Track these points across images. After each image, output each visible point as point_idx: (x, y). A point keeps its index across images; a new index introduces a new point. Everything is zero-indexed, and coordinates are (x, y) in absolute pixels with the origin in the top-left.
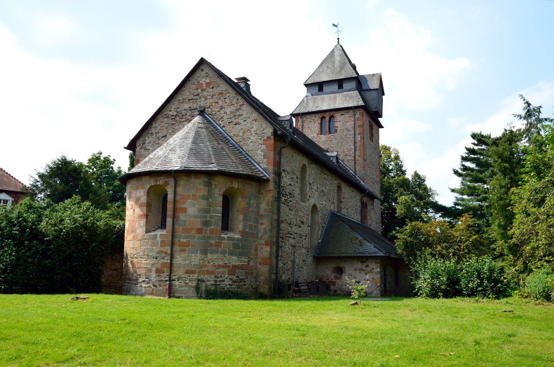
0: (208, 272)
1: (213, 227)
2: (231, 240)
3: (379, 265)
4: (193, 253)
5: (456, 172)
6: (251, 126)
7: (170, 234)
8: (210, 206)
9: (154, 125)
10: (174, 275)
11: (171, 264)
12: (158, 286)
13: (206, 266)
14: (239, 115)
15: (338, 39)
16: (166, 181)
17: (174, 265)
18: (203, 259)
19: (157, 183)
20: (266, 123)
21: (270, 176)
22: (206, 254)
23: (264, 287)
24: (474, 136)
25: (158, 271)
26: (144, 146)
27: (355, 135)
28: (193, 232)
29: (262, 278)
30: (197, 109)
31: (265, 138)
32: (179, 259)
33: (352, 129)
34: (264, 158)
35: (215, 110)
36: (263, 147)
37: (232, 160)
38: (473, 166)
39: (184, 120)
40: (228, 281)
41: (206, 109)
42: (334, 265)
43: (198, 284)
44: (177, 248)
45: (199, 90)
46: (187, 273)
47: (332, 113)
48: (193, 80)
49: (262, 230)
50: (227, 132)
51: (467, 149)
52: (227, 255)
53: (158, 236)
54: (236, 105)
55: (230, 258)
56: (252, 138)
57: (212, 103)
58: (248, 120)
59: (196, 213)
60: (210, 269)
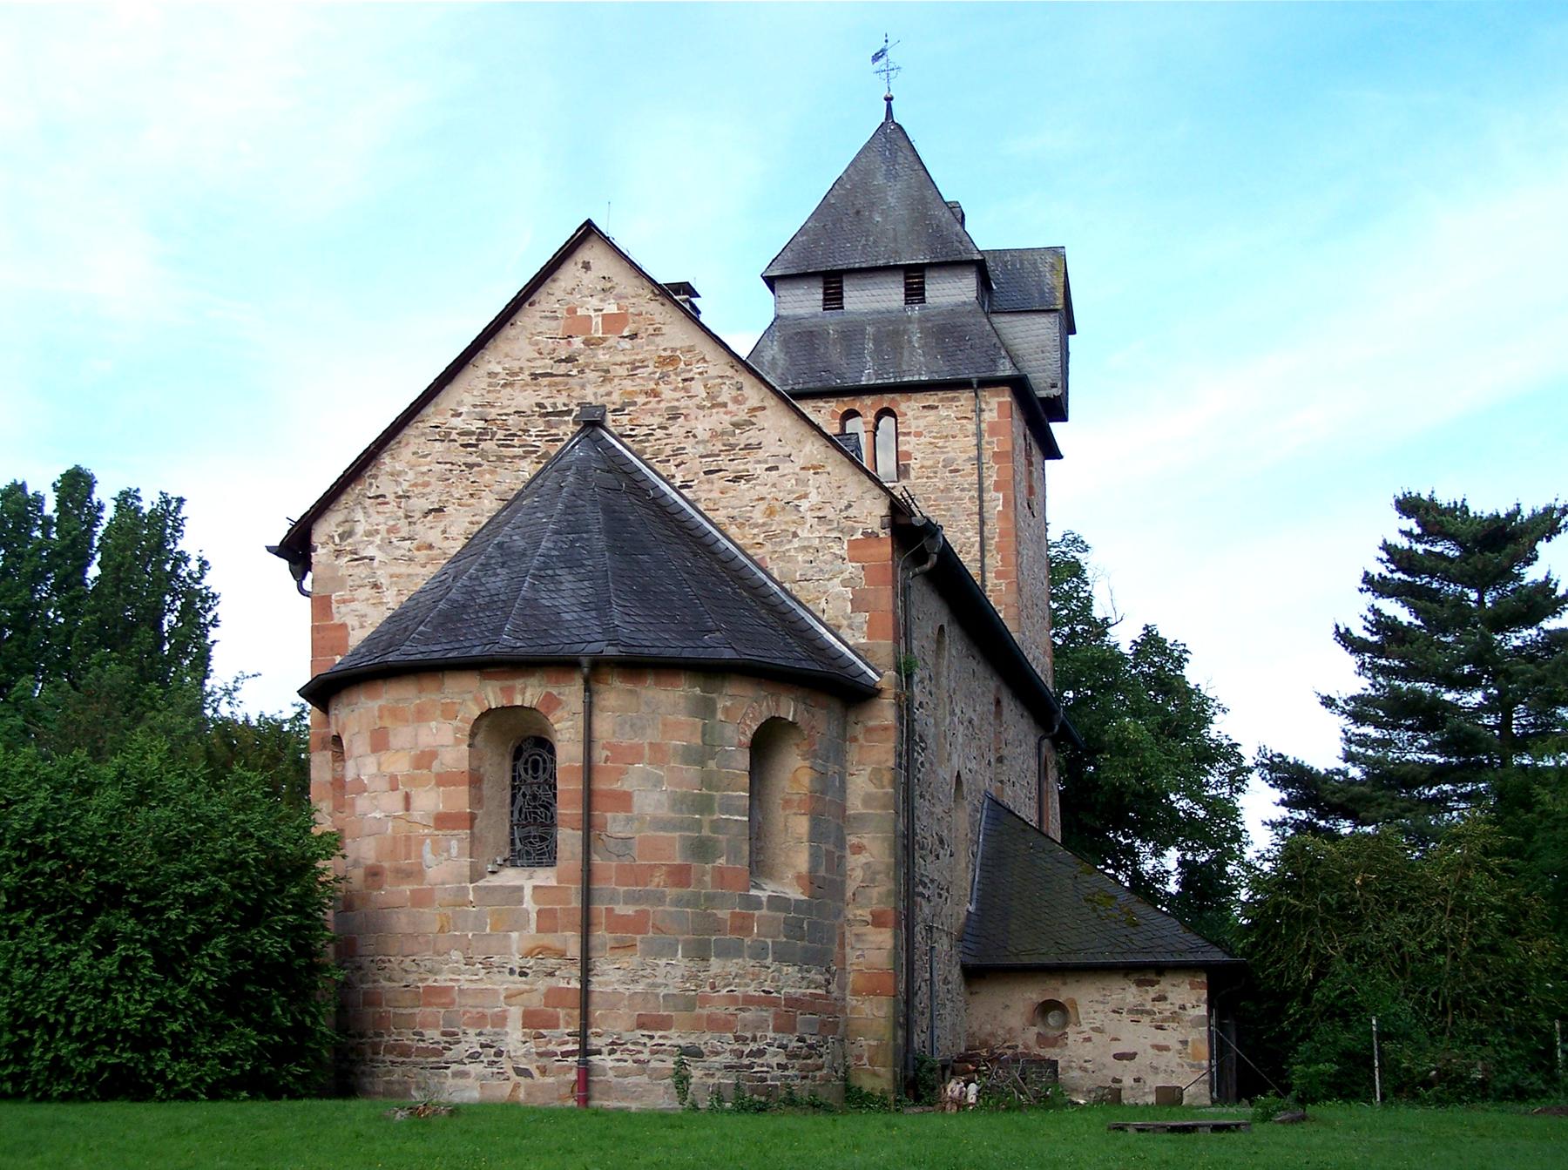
0: (714, 1024)
1: (722, 861)
2: (778, 909)
3: (1204, 994)
4: (659, 955)
5: (1346, 639)
6: (801, 490)
7: (575, 889)
8: (710, 788)
9: (387, 461)
10: (599, 1035)
11: (585, 992)
12: (536, 1073)
13: (705, 1000)
14: (748, 447)
15: (889, 99)
16: (549, 694)
17: (595, 998)
18: (693, 977)
19: (511, 698)
20: (861, 482)
21: (885, 679)
22: (705, 959)
23: (875, 1074)
24: (1408, 506)
25: (534, 1022)
26: (347, 545)
27: (981, 490)
28: (659, 878)
29: (865, 1043)
30: (569, 412)
31: (858, 536)
32: (610, 977)
33: (968, 467)
34: (857, 607)
35: (648, 420)
36: (851, 568)
37: (761, 618)
38: (1404, 615)
39: (519, 451)
40: (776, 1055)
41: (610, 417)
42: (1031, 994)
43: (681, 1063)
44: (600, 935)
45: (577, 343)
46: (641, 1026)
47: (886, 401)
48: (548, 299)
49: (859, 874)
50: (701, 507)
51: (1386, 547)
52: (770, 960)
53: (528, 892)
54: (731, 406)
55: (780, 971)
56: (803, 533)
57: (631, 393)
58: (785, 468)
59: (665, 813)
60: (719, 1011)
